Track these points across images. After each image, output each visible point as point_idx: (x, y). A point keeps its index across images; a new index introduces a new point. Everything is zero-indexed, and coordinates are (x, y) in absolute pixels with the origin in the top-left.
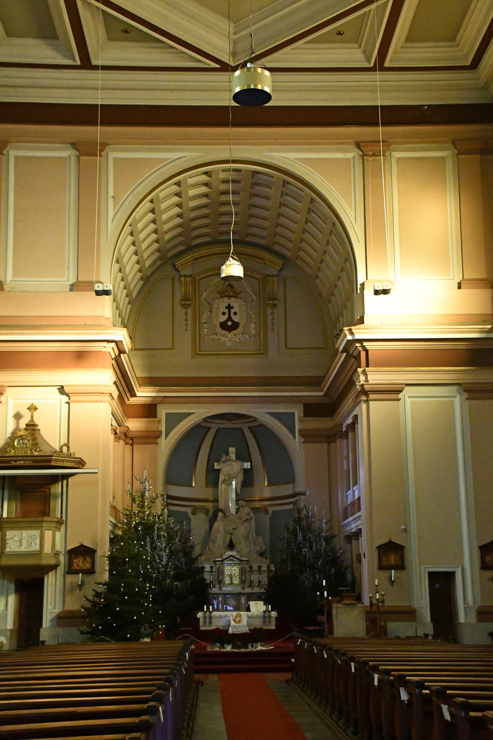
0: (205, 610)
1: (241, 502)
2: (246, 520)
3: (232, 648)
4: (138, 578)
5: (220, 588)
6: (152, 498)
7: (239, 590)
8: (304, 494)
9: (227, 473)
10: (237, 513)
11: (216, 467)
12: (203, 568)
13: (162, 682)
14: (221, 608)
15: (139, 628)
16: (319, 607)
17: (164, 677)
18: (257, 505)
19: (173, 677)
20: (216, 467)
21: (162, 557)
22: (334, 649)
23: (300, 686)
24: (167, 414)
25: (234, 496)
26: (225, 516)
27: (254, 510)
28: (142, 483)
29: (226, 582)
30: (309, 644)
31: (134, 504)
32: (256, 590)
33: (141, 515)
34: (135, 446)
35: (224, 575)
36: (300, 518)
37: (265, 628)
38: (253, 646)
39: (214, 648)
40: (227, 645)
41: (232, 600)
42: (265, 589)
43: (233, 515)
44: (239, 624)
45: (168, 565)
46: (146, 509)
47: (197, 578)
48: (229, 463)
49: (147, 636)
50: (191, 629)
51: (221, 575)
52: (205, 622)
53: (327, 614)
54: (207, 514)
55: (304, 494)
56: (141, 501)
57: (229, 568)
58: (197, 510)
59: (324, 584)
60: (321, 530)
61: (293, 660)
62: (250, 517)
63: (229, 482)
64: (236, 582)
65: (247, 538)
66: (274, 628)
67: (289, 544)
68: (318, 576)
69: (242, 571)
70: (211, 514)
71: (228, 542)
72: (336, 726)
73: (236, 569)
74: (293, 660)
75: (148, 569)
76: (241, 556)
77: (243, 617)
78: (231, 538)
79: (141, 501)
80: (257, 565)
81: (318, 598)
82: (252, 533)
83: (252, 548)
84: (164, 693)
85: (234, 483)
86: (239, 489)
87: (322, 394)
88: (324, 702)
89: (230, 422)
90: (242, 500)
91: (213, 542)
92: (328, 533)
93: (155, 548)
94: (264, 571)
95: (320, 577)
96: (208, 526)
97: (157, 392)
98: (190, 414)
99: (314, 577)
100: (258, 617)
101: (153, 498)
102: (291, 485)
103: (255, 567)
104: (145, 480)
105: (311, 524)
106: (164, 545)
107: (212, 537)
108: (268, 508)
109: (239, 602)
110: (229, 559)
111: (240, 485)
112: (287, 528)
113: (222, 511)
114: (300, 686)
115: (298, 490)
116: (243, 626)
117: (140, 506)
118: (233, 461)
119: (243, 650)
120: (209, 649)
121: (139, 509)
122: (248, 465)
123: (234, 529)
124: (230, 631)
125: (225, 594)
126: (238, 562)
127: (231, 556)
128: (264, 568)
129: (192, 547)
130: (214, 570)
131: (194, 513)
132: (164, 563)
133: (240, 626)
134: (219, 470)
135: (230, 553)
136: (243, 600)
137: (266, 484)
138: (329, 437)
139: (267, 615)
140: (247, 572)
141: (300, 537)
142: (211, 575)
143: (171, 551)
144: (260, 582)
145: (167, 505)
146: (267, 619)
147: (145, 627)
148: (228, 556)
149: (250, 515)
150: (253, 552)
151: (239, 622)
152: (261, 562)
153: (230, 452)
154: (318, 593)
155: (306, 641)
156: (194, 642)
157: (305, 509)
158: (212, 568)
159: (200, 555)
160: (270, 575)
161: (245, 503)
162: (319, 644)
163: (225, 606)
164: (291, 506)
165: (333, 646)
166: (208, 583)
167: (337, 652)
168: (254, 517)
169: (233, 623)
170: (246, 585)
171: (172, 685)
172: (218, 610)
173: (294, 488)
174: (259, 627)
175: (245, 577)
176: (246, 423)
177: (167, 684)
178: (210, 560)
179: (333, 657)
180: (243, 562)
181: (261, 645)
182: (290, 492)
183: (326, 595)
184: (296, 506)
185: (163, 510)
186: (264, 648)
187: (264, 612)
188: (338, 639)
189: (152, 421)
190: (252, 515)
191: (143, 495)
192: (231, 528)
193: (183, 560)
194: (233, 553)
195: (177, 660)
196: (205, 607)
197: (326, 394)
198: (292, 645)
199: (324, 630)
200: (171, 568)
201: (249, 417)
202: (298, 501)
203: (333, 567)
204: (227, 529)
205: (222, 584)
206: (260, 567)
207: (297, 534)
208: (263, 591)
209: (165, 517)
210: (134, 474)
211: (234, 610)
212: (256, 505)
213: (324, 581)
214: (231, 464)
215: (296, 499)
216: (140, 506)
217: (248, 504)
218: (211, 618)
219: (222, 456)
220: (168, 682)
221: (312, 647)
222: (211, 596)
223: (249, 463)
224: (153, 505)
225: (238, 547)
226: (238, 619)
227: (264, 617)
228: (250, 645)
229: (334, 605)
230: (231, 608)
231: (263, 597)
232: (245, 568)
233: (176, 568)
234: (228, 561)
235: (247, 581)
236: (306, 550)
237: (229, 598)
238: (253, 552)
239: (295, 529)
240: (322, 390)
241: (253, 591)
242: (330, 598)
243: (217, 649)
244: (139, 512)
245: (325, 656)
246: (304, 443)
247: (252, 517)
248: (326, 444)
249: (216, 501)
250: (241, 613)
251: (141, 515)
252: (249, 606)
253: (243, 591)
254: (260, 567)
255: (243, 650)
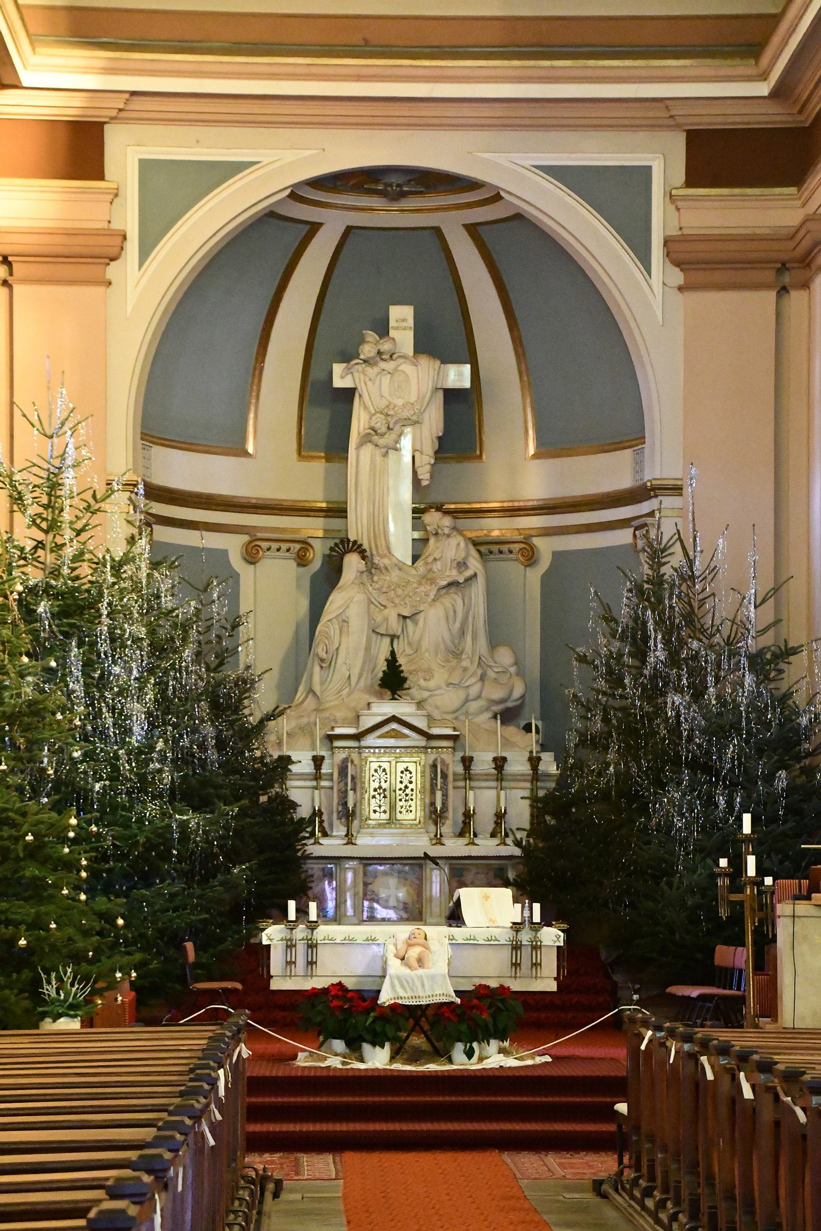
0: (292, 915)
1: (432, 519)
2: (453, 584)
3: (393, 1059)
4: (36, 794)
5: (350, 839)
6: (88, 496)
7: (420, 844)
8: (677, 490)
9: (382, 404)
10: (415, 558)
11: (341, 378)
12: (285, 761)
13: (127, 1173)
14: (350, 912)
15: (37, 983)
16: (723, 913)
17: (133, 1155)
18: (496, 527)
19: (168, 1156)
20: (338, 383)
21: (129, 717)
22: (781, 1067)
23: (650, 1203)
24: (145, 165)
25: (405, 493)
26: (371, 568)
27: (483, 549)
28: (51, 437)
29: (373, 816)
30: (687, 1047)
31: (17, 516)
32: (487, 846)
33: (49, 558)
34: (19, 289)
35: (364, 790)
36: (658, 581)
37: (516, 986)
38: (470, 1054)
39: (325, 1059)
40: (374, 1044)
41: (392, 881)
42: (518, 843)
43: (400, 566)
44: (421, 971)
45: (152, 748)
46: (68, 534)
47: (263, 799)
48: (389, 366)
49: (71, 1009)
50: (239, 986)
51: (354, 789)
52: (290, 963)
53: (755, 943)
54: (302, 560)
55: (677, 490)
56: (46, 507)
57: (385, 766)
58: (264, 545)
59: (747, 828)
60: (740, 626)
61: (622, 1107)
62: (468, 573)
63: (389, 439)
64: (411, 816)
65: (456, 653)
66: (552, 986)
67: (616, 680)
68: (722, 801)
69: (434, 779)
70: (316, 565)
71: (382, 666)
72: (638, 1208)
73: (412, 767)
74: (622, 1107)
75: (74, 762)
76: (430, 717)
77: (433, 944)
78: (393, 653)
79: (46, 507)
80: (490, 756)
81: (720, 882)
82: (474, 638)
83: (474, 691)
84: (133, 1210)
85: (406, 444)
86: (428, 468)
87: (763, 89)
88: (669, 1205)
89: (396, 206)
90: (439, 508)
91: (326, 664)
92: (768, 640)
93: (103, 682)
94: (517, 778)
95: (730, 803)
96: (304, 604)
97: (109, 71)
98: (236, 168)
99: (710, 802)
100: (491, 944)
101: (94, 496)
102: (628, 453)
103: (484, 762)
104: (63, 424)
105: (702, 602)
106: (135, 672)
107: (320, 650)
108: (536, 541)
109: (419, 889)
110: (386, 729)
111: (429, 447)
112: (609, 618)
113: (357, 548)
114: (650, 1203)
115: (655, 472)
116: (432, 978)
117: (44, 525)
118: (404, 357)
119: (432, 1067)
120: (303, 1061)
121: (40, 536)
122: (460, 375)
123: (405, 617)
124: (386, 998)
125: (366, 861)
126: (418, 740)
127: (394, 719)
128: (518, 765)
129: (245, 685)
130: (325, 769)
131: (251, 556)
132: (136, 738)
133: (421, 978)
134: (349, 395)
135: (385, 708)
136: (436, 881)
137: (532, 451)
138: (783, 267)
139: (525, 937)
140: (451, 777)
141: (658, 654)
142: (316, 788)
143: (163, 701)
144: (500, 817)
145: (149, 524)
146: (526, 952)
147: (60, 979)
148: (379, 719)
149: (467, 568)
150: (474, 706)
151: (420, 961)
152: (507, 743)
153: (392, 323)
154: (723, 862)
155: (672, 1033)
156: (253, 1035)
157: (677, 548)
158: (318, 761)
159: (272, 716)
160: (541, 793)
161: (447, 521)
162: (724, 1050)
163: (366, 903)
164: (624, 537)
165: (776, 1058)
166: (302, 820)
167: (792, 1077)
168: (481, 580)
169: (395, 967)
170: (447, 828)
171: (165, 1185)
172: (337, 919)
173: (639, 465)
174: (494, 984)
175: (445, 795)
176: (458, 207)
177: (147, 1178)
178: (312, 735)
179: (777, 1097)
180: (435, 743)
181: (501, 1051)
182: (624, 482)
183: (751, 871)
184: (646, 536)
185: (132, 541)
186: (511, 1062)
187: (517, 927)
188: (795, 1032)
189: (83, 191)
190: (475, 564)
191: (54, 486)
192: (392, 614)
193: (209, 730)
194: (402, 708)
195: (181, 1094)
196: (292, 905)
197: (777, 94)
198: (621, 1053)
199: (742, 1000)
200: (163, 759)
201: (472, 185)
202: (651, 514)
203: (786, 767)
204: (379, 619)
205: (356, 823)
206: (500, 763)
207: (646, 638)
208: (512, 850)
209: (139, 568)
210: (15, 400)
211: (401, 920)
212: (490, 531)
213: (747, 818)
214: (396, 369)
215: (645, 507)
216: (44, 525)
217: (462, 523)
218: (312, 946)
219: (362, 341)
220: (149, 1172)
221: (693, 1057)
222: (314, 868)
223: (467, 368)
224: (95, 520)
225: (417, 684)
226: (414, 953)
227: (516, 947)
228: (458, 1051)
229: (783, 909)
230: (391, 914)
231: (511, 875)
232: (443, 762)
233: (183, 760)
234: (380, 737)
235: (450, 814)
236: (677, 699)
237: (385, 874)
238: (474, 706)
239: (640, 623)
240: (763, 76)
241: (474, 851)
242: (768, 881)
243: (335, 1062)
244: (40, 545)
245: (748, 1093)
246: (680, 289)
247: (475, 575)
248: (773, 294)
249: (338, 511)
250: (427, 929)
251: (49, 558)
252: (458, 903)
253: (435, 851)
254: (500, 763)
255: (432, 1067)
